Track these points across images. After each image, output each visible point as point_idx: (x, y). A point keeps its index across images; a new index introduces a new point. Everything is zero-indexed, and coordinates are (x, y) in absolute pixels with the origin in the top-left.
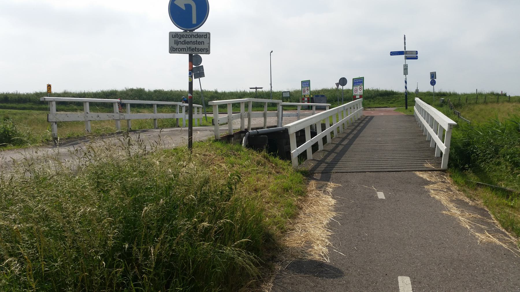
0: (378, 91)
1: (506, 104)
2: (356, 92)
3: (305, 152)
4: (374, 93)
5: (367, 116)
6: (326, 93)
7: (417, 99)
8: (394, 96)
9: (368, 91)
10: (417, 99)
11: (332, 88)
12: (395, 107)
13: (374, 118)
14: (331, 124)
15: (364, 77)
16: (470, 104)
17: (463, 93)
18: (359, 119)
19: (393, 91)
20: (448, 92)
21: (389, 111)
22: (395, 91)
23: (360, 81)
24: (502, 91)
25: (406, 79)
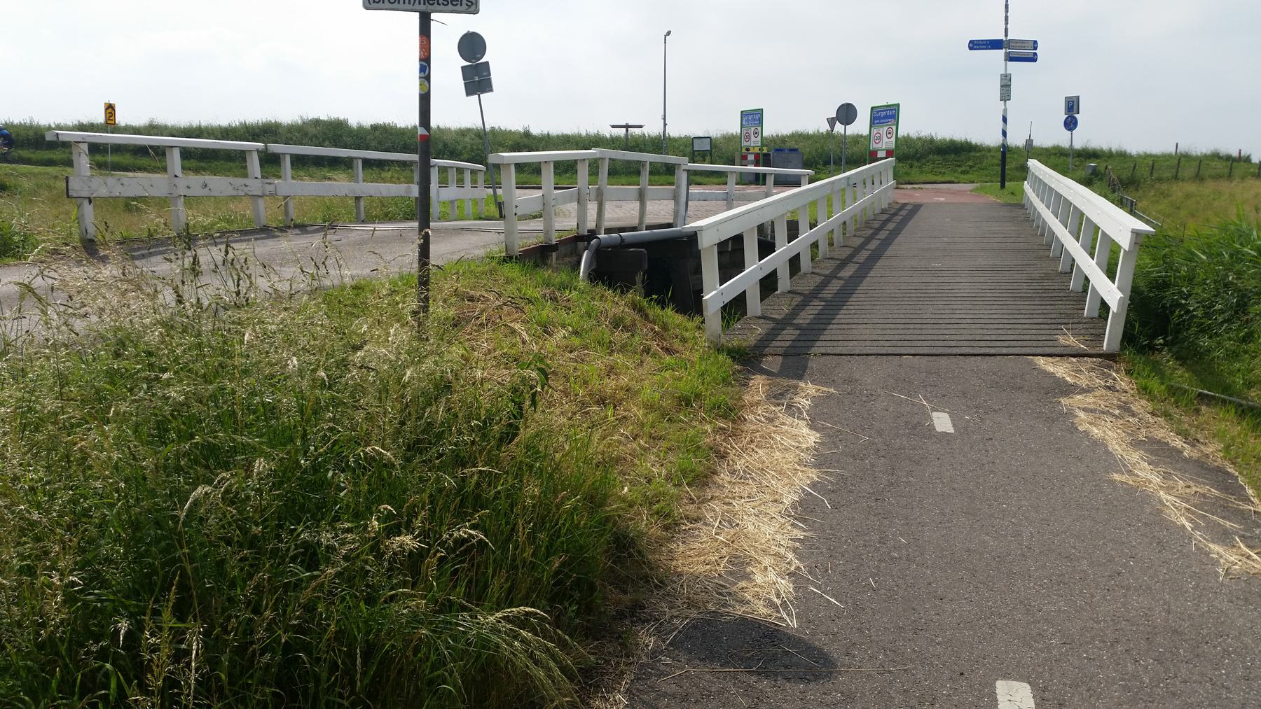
0: (932, 141)
5: (905, 205)
8: (973, 154)
9: (906, 142)
11: (818, 131)
12: (973, 182)
17: (1141, 153)
18: (883, 212)
25: (1005, 110)
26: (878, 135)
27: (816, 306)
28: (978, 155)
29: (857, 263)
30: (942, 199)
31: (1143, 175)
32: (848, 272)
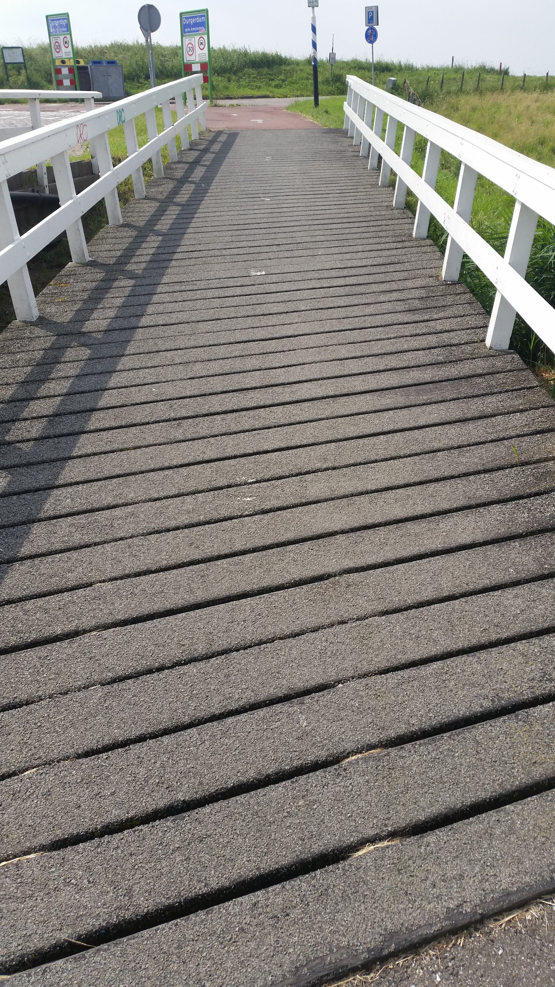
0: (246, 54)
1: (519, 95)
2: (190, 53)
3: (101, 204)
4: (238, 58)
5: (219, 133)
6: (121, 56)
7: (353, 80)
8: (283, 67)
9: (222, 54)
10: (353, 80)
11: (137, 42)
12: (286, 97)
13: (238, 140)
14: (120, 154)
15: (207, 11)
16: (449, 93)
17: (425, 66)
18: (193, 146)
19: (279, 54)
20: (395, 62)
21: (274, 111)
22: (283, 56)
23: (199, 20)
24: (501, 63)
25: (314, 18)
26: (190, 46)
27: (173, 212)
28: (288, 68)
29: (204, 166)
30: (260, 121)
31: (435, 88)
32: (199, 173)
